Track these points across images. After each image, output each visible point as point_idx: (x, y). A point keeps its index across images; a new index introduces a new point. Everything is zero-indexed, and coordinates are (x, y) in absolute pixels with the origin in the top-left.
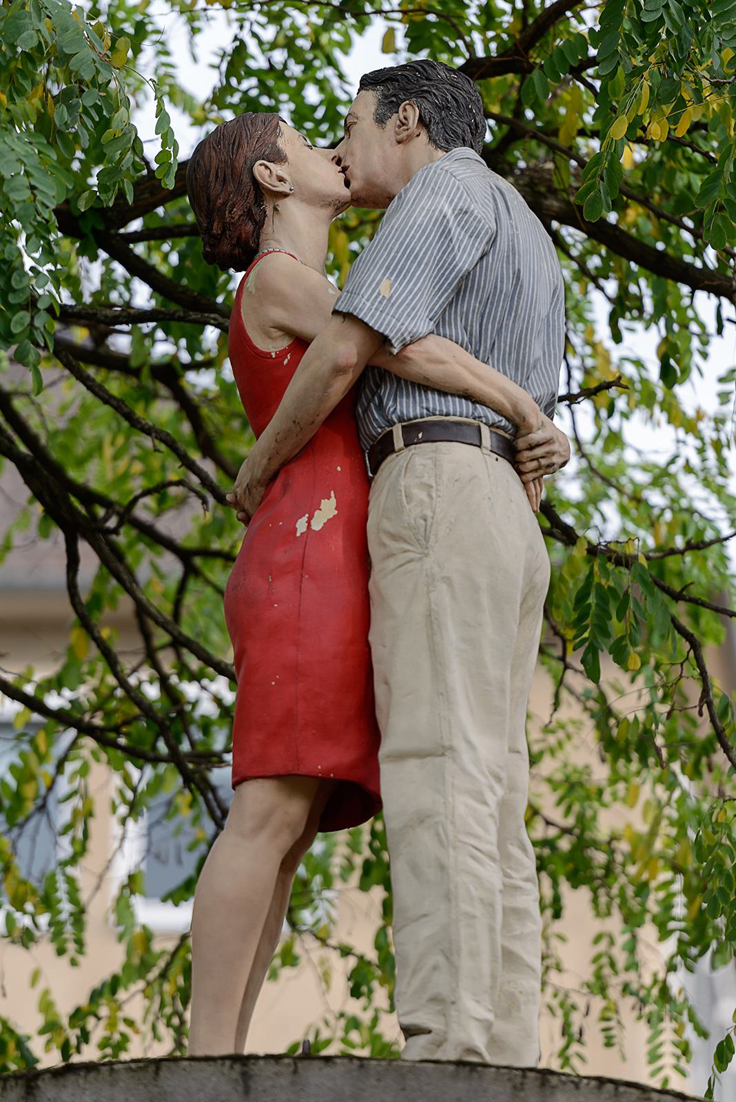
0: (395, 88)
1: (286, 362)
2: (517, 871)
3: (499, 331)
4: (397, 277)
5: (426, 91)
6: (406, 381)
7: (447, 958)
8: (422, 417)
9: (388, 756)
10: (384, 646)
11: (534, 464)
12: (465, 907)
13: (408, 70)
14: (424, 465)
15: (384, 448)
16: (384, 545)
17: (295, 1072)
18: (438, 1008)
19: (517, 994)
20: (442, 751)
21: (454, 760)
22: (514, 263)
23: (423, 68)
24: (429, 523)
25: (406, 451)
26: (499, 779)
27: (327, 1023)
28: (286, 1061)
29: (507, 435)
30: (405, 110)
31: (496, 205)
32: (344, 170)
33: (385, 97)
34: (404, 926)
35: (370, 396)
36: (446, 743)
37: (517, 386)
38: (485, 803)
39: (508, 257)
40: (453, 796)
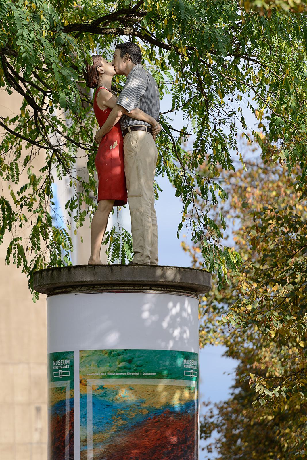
15: (126, 131)
20: (141, 196)
27: (76, 195)
32: (114, 67)
33: (122, 51)
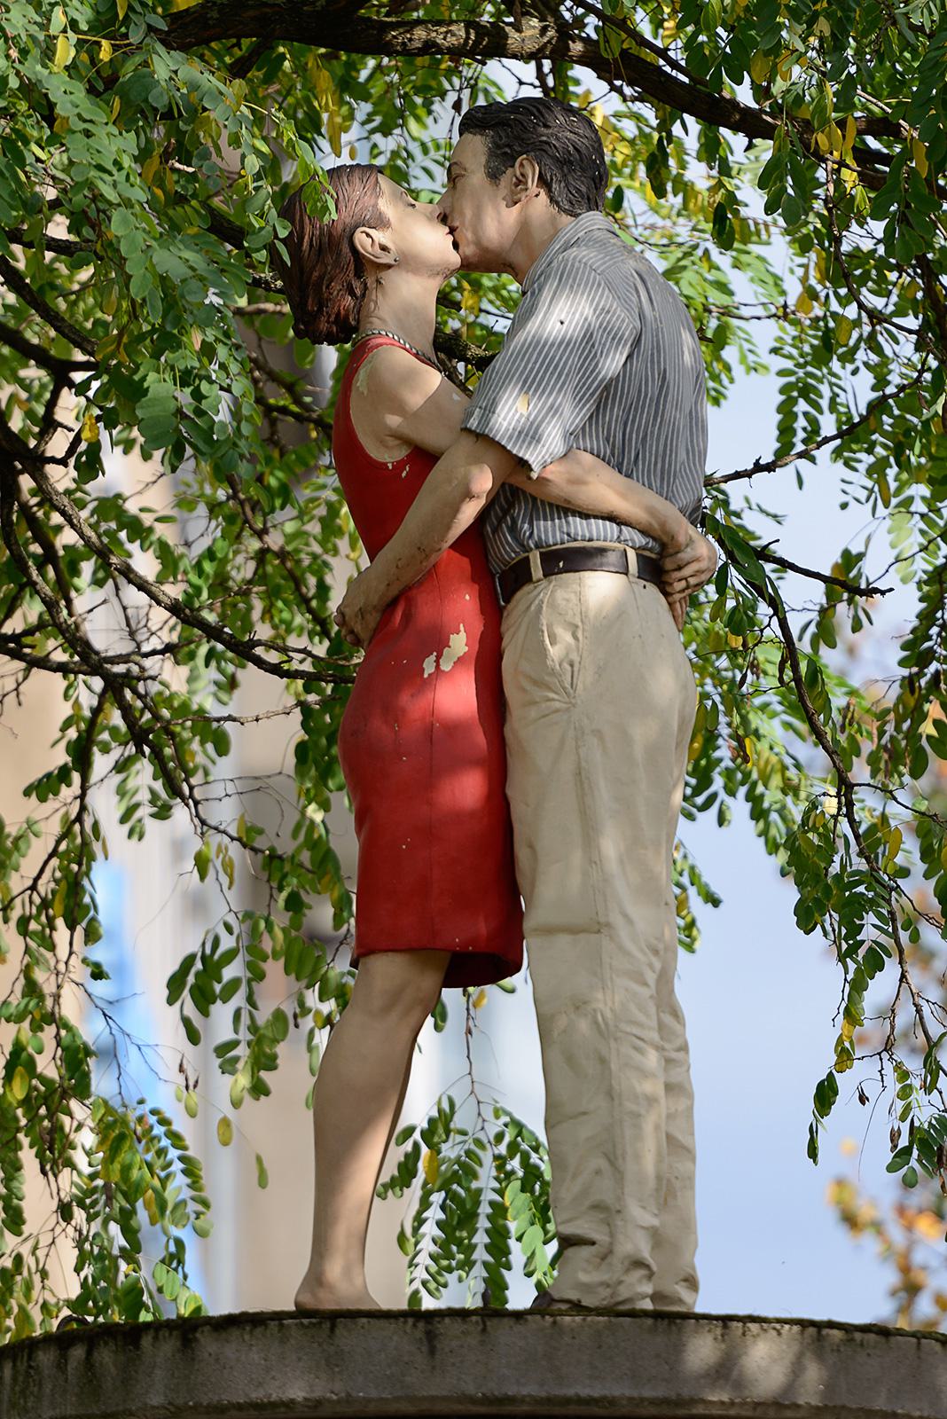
0: (507, 136)
1: (404, 474)
2: (669, 1041)
3: (645, 438)
4: (536, 391)
5: (546, 143)
6: (542, 502)
7: (612, 1163)
8: (562, 543)
9: (536, 930)
10: (527, 805)
11: (683, 584)
12: (630, 1106)
13: (521, 113)
14: (568, 600)
15: (518, 577)
16: (524, 690)
17: (484, 1330)
18: (602, 1216)
19: (673, 1180)
21: (611, 938)
22: (659, 362)
23: (538, 110)
24: (576, 669)
25: (544, 583)
26: (656, 952)
28: (474, 1318)
29: (653, 556)
30: (522, 165)
31: (639, 297)
32: (452, 231)
33: (498, 146)
34: (559, 1123)
35: (500, 514)
36: (602, 920)
37: (662, 499)
38: (645, 984)
39: (652, 354)
40: (611, 979)
